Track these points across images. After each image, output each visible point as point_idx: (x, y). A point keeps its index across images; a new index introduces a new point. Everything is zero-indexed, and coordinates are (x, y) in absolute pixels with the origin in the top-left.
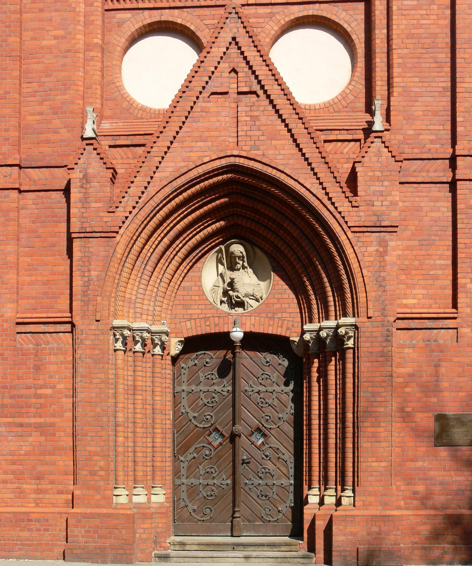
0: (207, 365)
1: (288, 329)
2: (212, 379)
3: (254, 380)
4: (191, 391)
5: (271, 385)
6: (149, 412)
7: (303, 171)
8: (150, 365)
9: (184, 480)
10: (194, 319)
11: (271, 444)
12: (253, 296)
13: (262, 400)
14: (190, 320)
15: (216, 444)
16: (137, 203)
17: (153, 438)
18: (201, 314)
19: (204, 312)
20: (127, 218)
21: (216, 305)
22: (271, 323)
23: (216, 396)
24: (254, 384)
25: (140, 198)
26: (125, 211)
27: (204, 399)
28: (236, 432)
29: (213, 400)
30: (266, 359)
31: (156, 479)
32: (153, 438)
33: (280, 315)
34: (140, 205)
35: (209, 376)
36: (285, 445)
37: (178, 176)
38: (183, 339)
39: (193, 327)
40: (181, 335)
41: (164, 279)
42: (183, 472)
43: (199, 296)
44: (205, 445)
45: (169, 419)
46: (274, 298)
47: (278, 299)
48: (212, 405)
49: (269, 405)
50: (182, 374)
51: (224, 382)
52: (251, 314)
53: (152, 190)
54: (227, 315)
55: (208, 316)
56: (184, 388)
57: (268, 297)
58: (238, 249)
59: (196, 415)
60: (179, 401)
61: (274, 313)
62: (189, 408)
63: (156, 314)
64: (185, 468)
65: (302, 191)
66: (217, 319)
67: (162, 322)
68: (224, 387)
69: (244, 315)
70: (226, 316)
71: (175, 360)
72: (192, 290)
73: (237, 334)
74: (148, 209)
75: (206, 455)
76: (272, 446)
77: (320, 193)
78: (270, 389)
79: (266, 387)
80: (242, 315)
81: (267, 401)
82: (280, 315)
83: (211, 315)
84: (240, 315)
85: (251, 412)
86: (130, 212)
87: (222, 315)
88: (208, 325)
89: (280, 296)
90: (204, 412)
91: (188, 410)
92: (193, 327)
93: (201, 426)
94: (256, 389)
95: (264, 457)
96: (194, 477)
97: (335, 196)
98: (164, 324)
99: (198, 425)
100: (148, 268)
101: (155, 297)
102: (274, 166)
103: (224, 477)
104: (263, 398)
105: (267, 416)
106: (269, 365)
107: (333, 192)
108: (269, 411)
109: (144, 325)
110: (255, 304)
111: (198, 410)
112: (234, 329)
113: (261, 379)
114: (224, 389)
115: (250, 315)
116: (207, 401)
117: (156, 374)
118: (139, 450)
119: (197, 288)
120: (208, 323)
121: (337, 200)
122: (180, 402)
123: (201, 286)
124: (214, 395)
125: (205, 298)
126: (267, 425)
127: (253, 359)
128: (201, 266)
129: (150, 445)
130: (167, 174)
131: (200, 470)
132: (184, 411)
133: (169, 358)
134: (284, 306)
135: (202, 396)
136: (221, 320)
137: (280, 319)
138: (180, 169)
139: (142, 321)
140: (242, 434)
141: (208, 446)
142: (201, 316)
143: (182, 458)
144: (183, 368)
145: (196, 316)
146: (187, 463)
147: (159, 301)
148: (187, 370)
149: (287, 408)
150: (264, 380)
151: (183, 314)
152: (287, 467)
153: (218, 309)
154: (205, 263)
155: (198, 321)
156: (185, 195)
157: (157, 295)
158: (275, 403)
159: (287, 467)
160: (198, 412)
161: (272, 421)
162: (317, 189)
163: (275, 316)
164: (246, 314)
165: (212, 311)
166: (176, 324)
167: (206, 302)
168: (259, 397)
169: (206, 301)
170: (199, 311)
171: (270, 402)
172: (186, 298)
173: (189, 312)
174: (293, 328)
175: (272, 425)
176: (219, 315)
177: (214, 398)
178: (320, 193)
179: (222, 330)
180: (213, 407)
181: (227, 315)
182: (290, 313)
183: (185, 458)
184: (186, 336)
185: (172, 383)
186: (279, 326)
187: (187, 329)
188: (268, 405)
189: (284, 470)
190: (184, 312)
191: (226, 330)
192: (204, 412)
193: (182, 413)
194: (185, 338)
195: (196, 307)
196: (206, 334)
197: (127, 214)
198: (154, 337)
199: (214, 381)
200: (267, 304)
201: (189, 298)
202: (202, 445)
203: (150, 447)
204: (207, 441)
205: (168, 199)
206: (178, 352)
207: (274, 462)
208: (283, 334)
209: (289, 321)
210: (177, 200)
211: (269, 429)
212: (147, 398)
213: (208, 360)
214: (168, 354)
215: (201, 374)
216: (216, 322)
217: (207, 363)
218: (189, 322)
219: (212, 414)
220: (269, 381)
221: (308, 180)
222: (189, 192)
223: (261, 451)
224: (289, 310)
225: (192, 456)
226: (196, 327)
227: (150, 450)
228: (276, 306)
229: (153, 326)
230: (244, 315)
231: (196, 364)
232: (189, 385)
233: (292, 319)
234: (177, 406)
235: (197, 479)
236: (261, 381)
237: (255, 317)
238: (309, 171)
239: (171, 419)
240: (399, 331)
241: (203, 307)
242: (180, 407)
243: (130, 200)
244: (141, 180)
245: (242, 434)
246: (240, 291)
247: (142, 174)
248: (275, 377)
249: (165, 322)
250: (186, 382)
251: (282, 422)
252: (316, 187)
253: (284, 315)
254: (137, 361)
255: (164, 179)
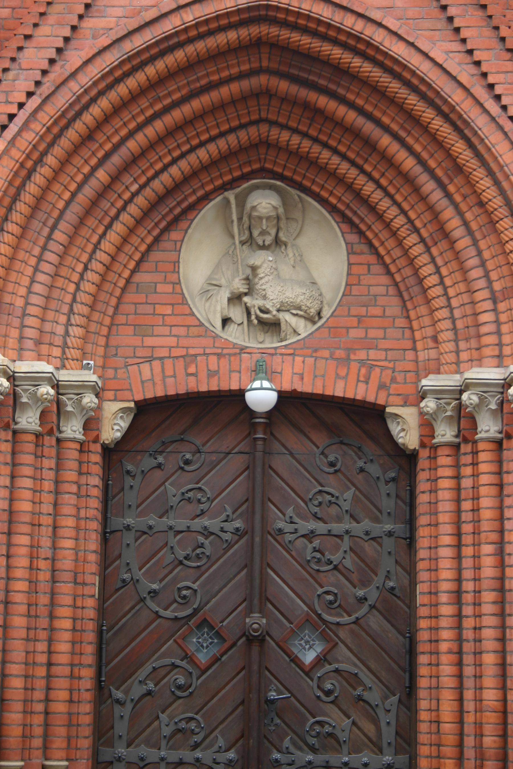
0: (187, 468)
1: (382, 387)
2: (199, 501)
3: (297, 508)
4: (146, 530)
5: (339, 519)
6: (44, 576)
7: (427, 24)
8: (52, 463)
9: (121, 750)
10: (161, 359)
11: (338, 661)
12: (299, 308)
13: (318, 555)
14: (150, 360)
15: (203, 658)
16: (38, 83)
17: (50, 641)
18: (177, 347)
19: (184, 342)
20: (11, 117)
21: (212, 328)
22: (343, 372)
23: (207, 542)
24: (299, 515)
25: (44, 72)
26: (8, 102)
27: (177, 549)
28: (255, 631)
29: (198, 551)
30: (326, 457)
31: (55, 746)
32: (50, 641)
33: (362, 355)
34: (46, 89)
35: (190, 494)
36: (373, 667)
37: (136, 26)
38: (132, 405)
39: (158, 379)
40: (127, 394)
41: (95, 265)
42: (121, 728)
43: (173, 305)
44: (178, 662)
45: (93, 596)
46: (349, 315)
47: (360, 317)
48: (194, 564)
49: (336, 568)
50: (127, 487)
51: (225, 510)
52: (293, 352)
53: (74, 58)
54: (238, 351)
55: (192, 351)
56: (129, 521)
57: (335, 314)
58: (264, 202)
59: (155, 586)
60: (116, 553)
61: (350, 350)
62: (140, 569)
63: (70, 344)
64: (127, 718)
65: (424, 68)
66: (213, 359)
67: (85, 362)
68: (226, 521)
69: (279, 351)
70: (235, 354)
71: (110, 452)
72: (156, 292)
73: (261, 396)
74: (63, 100)
75: (179, 687)
76: (342, 666)
77: (466, 74)
78: (337, 528)
79: (326, 523)
80: (272, 351)
81: (328, 556)
82: (362, 355)
83: (201, 351)
84: (269, 351)
85: (290, 583)
86: (21, 105)
87: (225, 351)
88: (192, 374)
89: (363, 311)
90: (175, 581)
91: (139, 574)
92: (158, 379)
93: (168, 614)
94: (307, 526)
95: (319, 693)
96: (148, 743)
97: (502, 80)
98: (87, 367)
99: (162, 612)
100: (59, 236)
101: (71, 306)
102: (360, 10)
103: (221, 742)
104: (318, 551)
105: (327, 593)
106: (336, 471)
107: (498, 73)
108: (332, 581)
109: (44, 367)
110: (305, 329)
111: (161, 576)
112: (257, 384)
113: (316, 503)
114: (227, 526)
115: (291, 351)
116: (184, 553)
117: (450, 463)
118: (15, 672)
119: (169, 288)
120: (192, 369)
121: (506, 89)
122: (120, 556)
123: (179, 283)
124: (201, 539)
125: (188, 312)
126: (330, 615)
127: (297, 456)
128: (179, 238)
129: (42, 659)
130: (110, 22)
131: (163, 726)
132: (126, 576)
133: (98, 448)
134: (372, 333)
135: (173, 541)
136: (224, 362)
137: (362, 362)
138: (140, 12)
139: (39, 358)
140: (267, 638)
141: (184, 664)
142: (177, 352)
143: (119, 695)
144: (128, 472)
145: (164, 353)
146: (129, 706)
147: (79, 314)
148: (139, 478)
149: (376, 575)
150: (324, 506)
151: (135, 347)
152: (375, 721)
153: (217, 336)
154: (190, 231)
155: (168, 363)
156: (151, 71)
157: (74, 300)
158: (348, 563)
159: (375, 721)
160: (161, 581)
161: (340, 606)
162: (459, 64)
163: (352, 357)
164: (283, 351)
165: (204, 342)
166: (116, 369)
167: (190, 321)
168: (310, 546)
169: (190, 318)
170: (172, 341)
171: (336, 558)
172: (141, 309)
173: (149, 341)
174: (394, 385)
175: (343, 617)
176: (219, 351)
177: (202, 546)
178: (466, 74)
179: (224, 387)
180: (198, 567)
181: (238, 351)
182: (386, 350)
183: (126, 692)
184: (139, 397)
185: (100, 508)
186: (362, 379)
187: (143, 382)
188: (331, 567)
189: (369, 728)
190: (137, 341)
191: (234, 386)
192: (175, 581)
193: (124, 581)
194: (136, 403)
195: (166, 330)
196: (187, 394)
197: (13, 109)
198: (64, 398)
199: (202, 506)
200: (333, 329)
201: (149, 309)
202: (168, 661)
203: (41, 665)
204: (180, 651)
205: (112, 79)
206: (119, 435)
207: (345, 708)
208: (371, 399)
209: (383, 368)
210: (132, 82)
211: (333, 627)
212: (42, 543)
213: (188, 456)
214: (96, 440)
215: (171, 489)
216: (211, 368)
217: (187, 462)
218: (147, 365)
219: (195, 586)
220: (333, 510)
221: (439, 43)
222: (160, 65)
223: (312, 680)
224: (383, 344)
225: (144, 689)
226: (164, 377)
227: (42, 672)
228: (354, 333)
229: (63, 372)
230: (279, 351)
231: (160, 464)
232: (141, 514)
233: (391, 365)
234: (110, 566)
235: (152, 747)
236: (316, 509)
237: (305, 356)
238: (442, 24)
239: (97, 597)
240: (318, 444)
241: (182, 331)
242: (118, 568)
243: (22, 77)
244: (50, 34)
245: (267, 638)
246: (271, 295)
247: (51, 19)
248: (349, 501)
249: (92, 362)
250: (134, 507)
251: (365, 609)
252: (457, 60)
253: (372, 354)
254: (21, 452)
255: (101, 32)
